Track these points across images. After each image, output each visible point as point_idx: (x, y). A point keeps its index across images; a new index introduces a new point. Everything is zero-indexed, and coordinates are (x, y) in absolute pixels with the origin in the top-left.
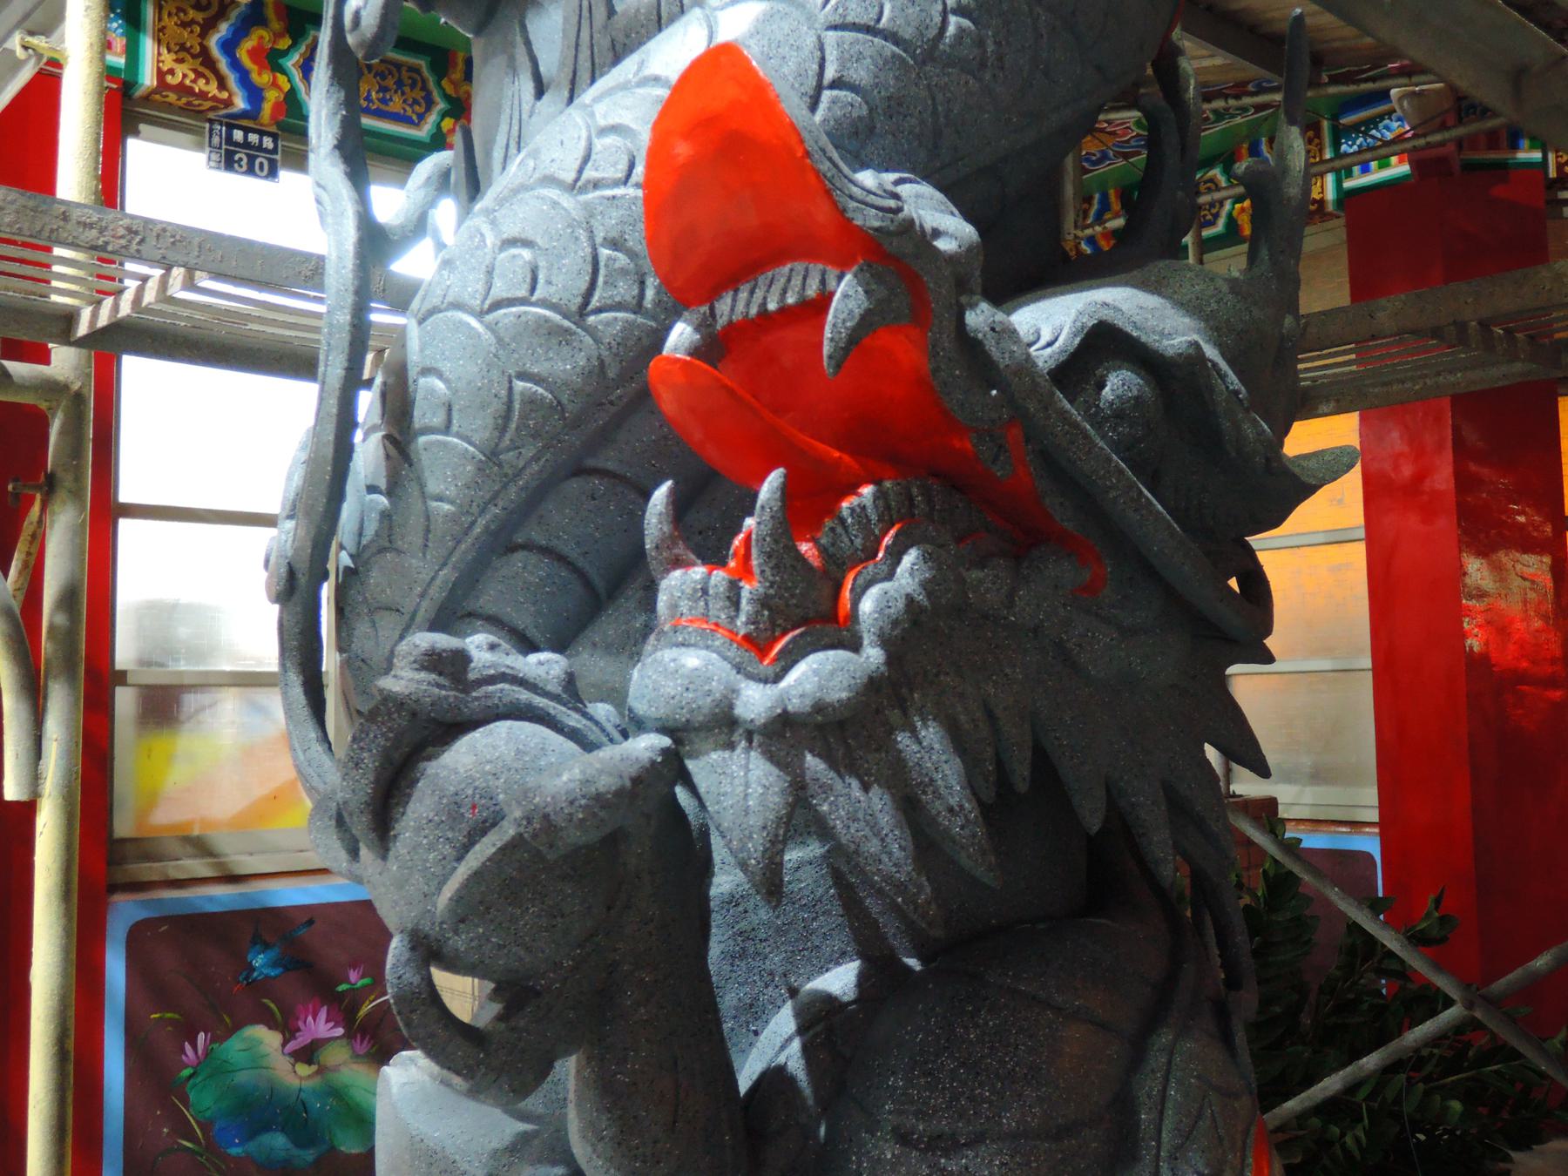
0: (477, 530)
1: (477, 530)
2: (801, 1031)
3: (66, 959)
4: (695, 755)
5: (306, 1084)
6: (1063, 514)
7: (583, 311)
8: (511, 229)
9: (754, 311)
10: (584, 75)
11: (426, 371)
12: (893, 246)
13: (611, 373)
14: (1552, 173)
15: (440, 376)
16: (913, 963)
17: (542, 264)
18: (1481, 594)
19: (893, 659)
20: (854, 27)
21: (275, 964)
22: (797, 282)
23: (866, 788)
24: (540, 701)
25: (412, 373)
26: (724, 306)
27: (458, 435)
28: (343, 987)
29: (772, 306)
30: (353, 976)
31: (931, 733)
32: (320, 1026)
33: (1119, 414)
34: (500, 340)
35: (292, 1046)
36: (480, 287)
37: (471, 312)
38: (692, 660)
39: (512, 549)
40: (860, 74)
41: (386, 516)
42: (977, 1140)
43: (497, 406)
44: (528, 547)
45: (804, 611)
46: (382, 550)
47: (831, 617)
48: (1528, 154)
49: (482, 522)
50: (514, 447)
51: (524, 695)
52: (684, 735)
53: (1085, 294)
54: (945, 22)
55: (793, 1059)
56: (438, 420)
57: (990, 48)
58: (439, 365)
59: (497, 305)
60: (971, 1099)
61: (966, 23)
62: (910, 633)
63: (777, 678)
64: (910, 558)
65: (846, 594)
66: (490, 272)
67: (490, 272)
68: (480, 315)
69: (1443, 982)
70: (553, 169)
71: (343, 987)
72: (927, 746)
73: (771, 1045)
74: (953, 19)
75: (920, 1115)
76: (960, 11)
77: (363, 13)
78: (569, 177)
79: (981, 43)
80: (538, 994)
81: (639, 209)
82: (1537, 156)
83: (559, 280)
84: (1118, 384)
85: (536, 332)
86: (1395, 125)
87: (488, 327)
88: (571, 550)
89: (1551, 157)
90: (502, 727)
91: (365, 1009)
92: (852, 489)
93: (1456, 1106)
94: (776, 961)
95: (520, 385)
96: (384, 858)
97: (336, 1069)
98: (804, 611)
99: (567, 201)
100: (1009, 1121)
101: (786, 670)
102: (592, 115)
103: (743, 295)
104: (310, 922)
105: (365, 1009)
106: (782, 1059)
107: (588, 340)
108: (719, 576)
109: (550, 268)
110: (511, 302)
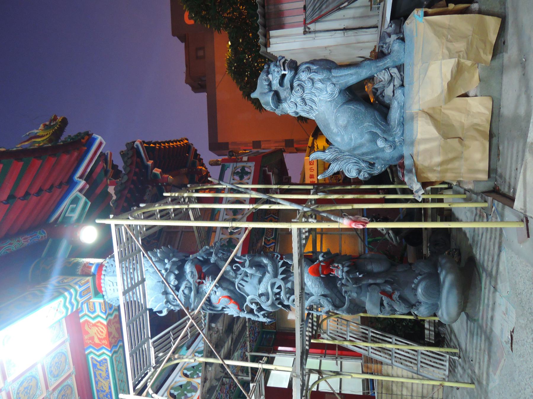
52: (343, 272)
62: (338, 263)
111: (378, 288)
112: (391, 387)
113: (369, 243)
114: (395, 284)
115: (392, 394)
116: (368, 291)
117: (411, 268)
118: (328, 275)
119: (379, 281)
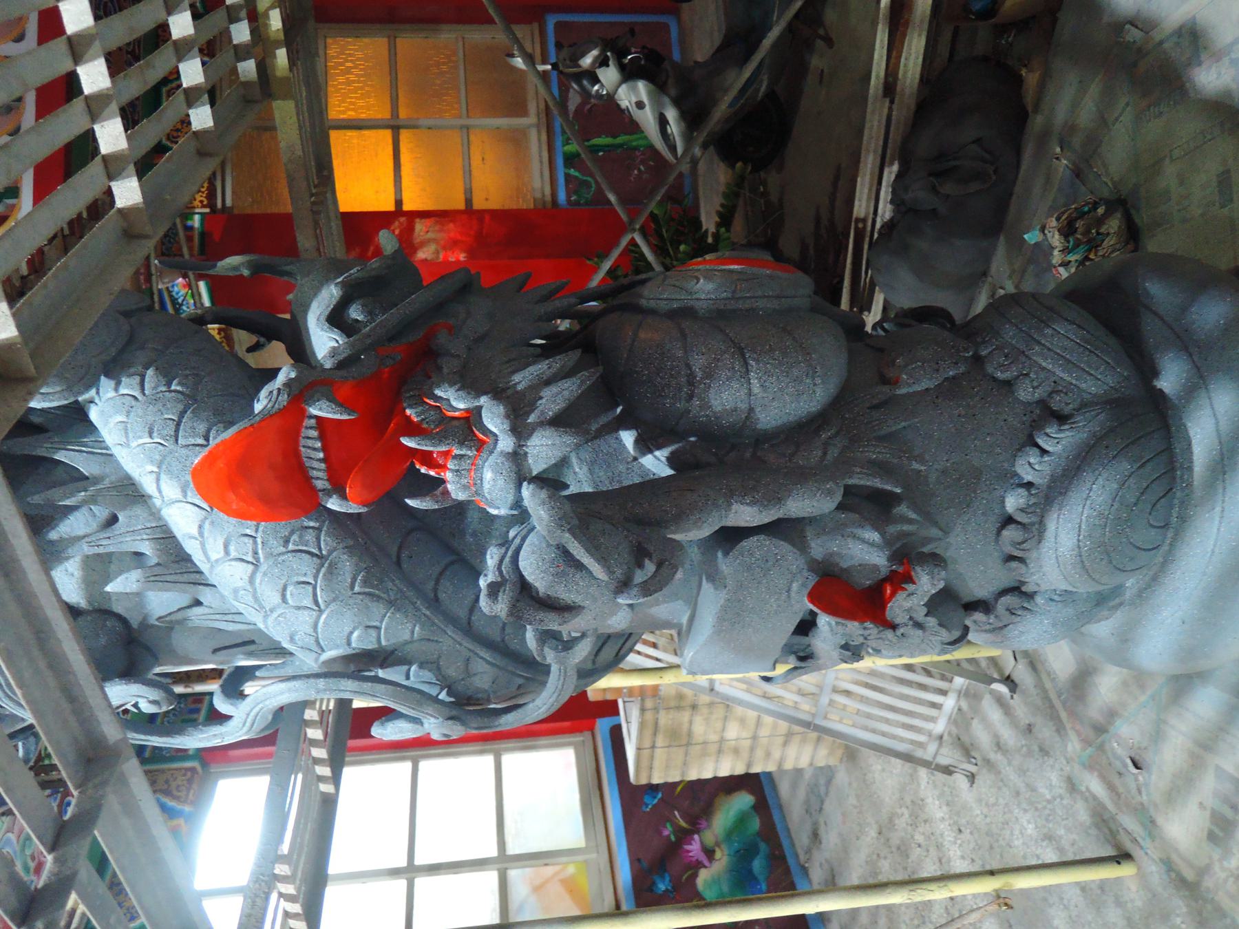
0: (428, 613)
1: (428, 613)
2: (651, 452)
3: (658, 911)
4: (530, 471)
5: (726, 852)
6: (415, 336)
7: (320, 557)
8: (277, 599)
9: (323, 466)
10: (193, 577)
11: (349, 644)
12: (296, 391)
13: (351, 543)
14: (207, 210)
15: (351, 633)
16: (619, 410)
17: (295, 579)
18: (437, 252)
19: (485, 393)
20: (177, 431)
21: (663, 877)
22: (310, 443)
23: (541, 398)
24: (510, 553)
25: (349, 651)
26: (320, 484)
27: (381, 622)
28: (673, 838)
29: (321, 455)
30: (666, 833)
31: (517, 378)
32: (694, 848)
33: (370, 313)
34: (334, 600)
35: (706, 862)
36: (306, 613)
37: (319, 617)
38: (488, 475)
39: (437, 599)
40: (201, 428)
41: (422, 666)
42: (688, 366)
43: (367, 600)
44: (435, 590)
45: (468, 430)
46: (439, 668)
47: (467, 419)
48: (196, 221)
49: (424, 610)
50: (387, 592)
51: (507, 559)
52: (521, 476)
53: (312, 331)
54: (175, 391)
55: (662, 454)
56: (373, 633)
57: (188, 372)
58: (346, 634)
59: (316, 603)
60: (672, 369)
61: (175, 382)
62: (471, 384)
63: (495, 435)
64: (438, 392)
65: (457, 414)
66: (298, 608)
67: (298, 608)
68: (321, 611)
69: (624, 242)
70: (246, 578)
71: (673, 838)
72: (521, 380)
73: (656, 464)
74: (173, 388)
75: (680, 390)
76: (169, 384)
77: (151, 698)
78: (251, 567)
79: (187, 376)
80: (640, 543)
81: (271, 525)
82: (197, 217)
83: (304, 569)
84: (355, 313)
85: (330, 580)
86: (176, 289)
87: (327, 607)
88: (438, 569)
89: (197, 210)
90: (522, 564)
91: (683, 824)
92: (408, 418)
93: (682, 247)
94: (622, 468)
95: (357, 589)
96: (584, 608)
97: (716, 836)
98: (468, 430)
99: (263, 568)
100: (680, 354)
101: (491, 432)
102: (217, 561)
103: (315, 473)
104: (639, 860)
105: (683, 824)
106: (664, 459)
107: (334, 554)
108: (450, 465)
109: (297, 574)
110: (315, 595)
111: (785, 547)
112: (686, 726)
113: (570, 160)
114: (903, 509)
115: (688, 744)
116: (714, 577)
117: (978, 360)
118: (388, 502)
119: (799, 505)
